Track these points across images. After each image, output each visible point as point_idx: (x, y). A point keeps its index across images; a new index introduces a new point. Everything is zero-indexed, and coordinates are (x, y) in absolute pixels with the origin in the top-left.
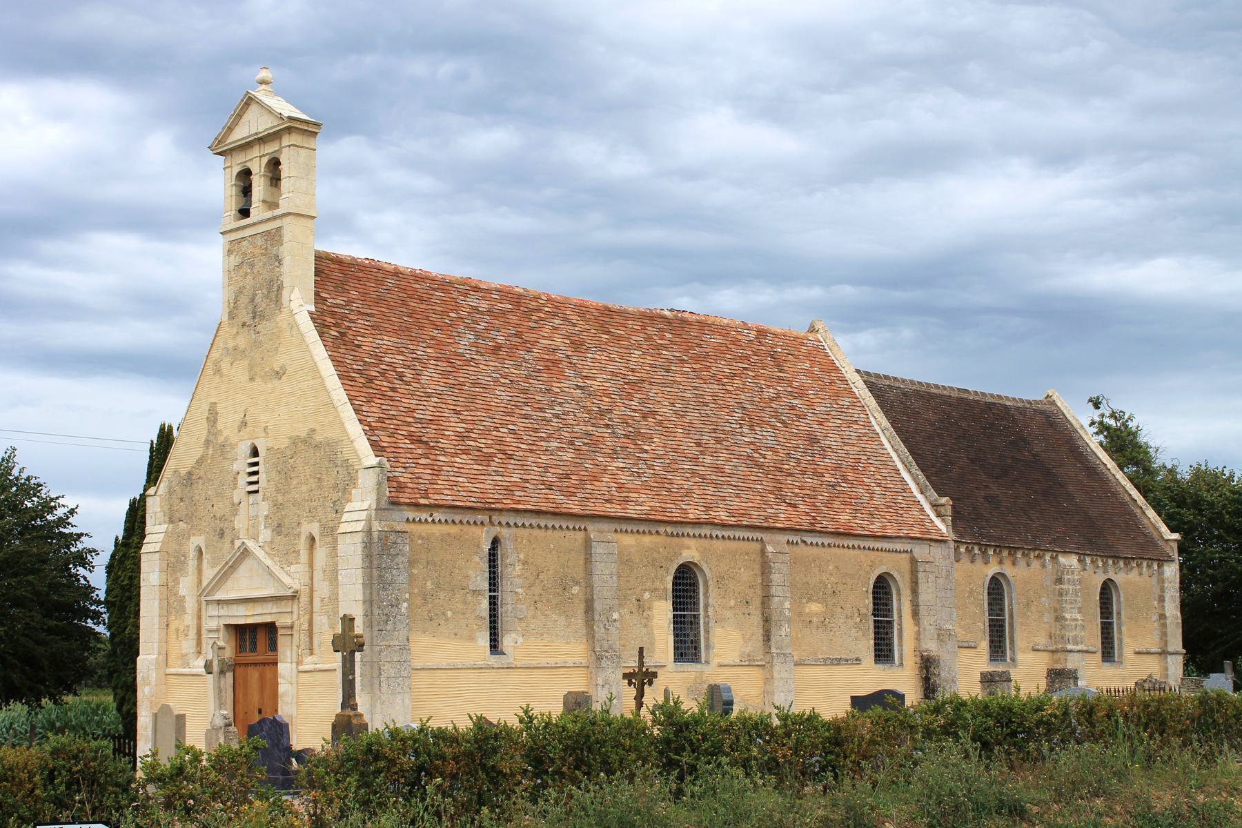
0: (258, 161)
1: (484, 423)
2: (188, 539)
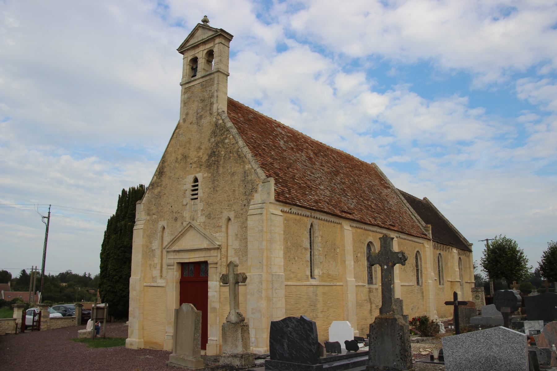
0: (202, 53)
2: (157, 223)
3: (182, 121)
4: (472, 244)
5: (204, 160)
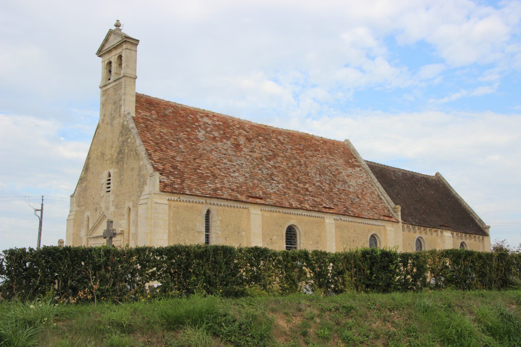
0: (114, 58)
1: (206, 164)
3: (101, 122)
4: (488, 227)
5: (114, 157)
